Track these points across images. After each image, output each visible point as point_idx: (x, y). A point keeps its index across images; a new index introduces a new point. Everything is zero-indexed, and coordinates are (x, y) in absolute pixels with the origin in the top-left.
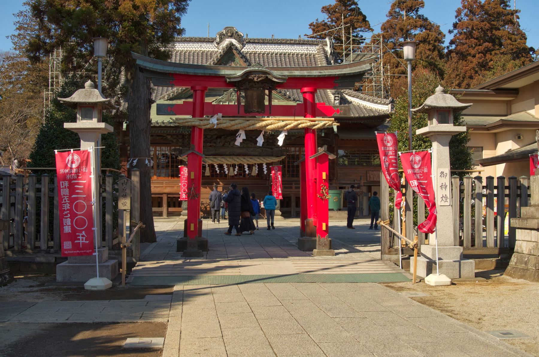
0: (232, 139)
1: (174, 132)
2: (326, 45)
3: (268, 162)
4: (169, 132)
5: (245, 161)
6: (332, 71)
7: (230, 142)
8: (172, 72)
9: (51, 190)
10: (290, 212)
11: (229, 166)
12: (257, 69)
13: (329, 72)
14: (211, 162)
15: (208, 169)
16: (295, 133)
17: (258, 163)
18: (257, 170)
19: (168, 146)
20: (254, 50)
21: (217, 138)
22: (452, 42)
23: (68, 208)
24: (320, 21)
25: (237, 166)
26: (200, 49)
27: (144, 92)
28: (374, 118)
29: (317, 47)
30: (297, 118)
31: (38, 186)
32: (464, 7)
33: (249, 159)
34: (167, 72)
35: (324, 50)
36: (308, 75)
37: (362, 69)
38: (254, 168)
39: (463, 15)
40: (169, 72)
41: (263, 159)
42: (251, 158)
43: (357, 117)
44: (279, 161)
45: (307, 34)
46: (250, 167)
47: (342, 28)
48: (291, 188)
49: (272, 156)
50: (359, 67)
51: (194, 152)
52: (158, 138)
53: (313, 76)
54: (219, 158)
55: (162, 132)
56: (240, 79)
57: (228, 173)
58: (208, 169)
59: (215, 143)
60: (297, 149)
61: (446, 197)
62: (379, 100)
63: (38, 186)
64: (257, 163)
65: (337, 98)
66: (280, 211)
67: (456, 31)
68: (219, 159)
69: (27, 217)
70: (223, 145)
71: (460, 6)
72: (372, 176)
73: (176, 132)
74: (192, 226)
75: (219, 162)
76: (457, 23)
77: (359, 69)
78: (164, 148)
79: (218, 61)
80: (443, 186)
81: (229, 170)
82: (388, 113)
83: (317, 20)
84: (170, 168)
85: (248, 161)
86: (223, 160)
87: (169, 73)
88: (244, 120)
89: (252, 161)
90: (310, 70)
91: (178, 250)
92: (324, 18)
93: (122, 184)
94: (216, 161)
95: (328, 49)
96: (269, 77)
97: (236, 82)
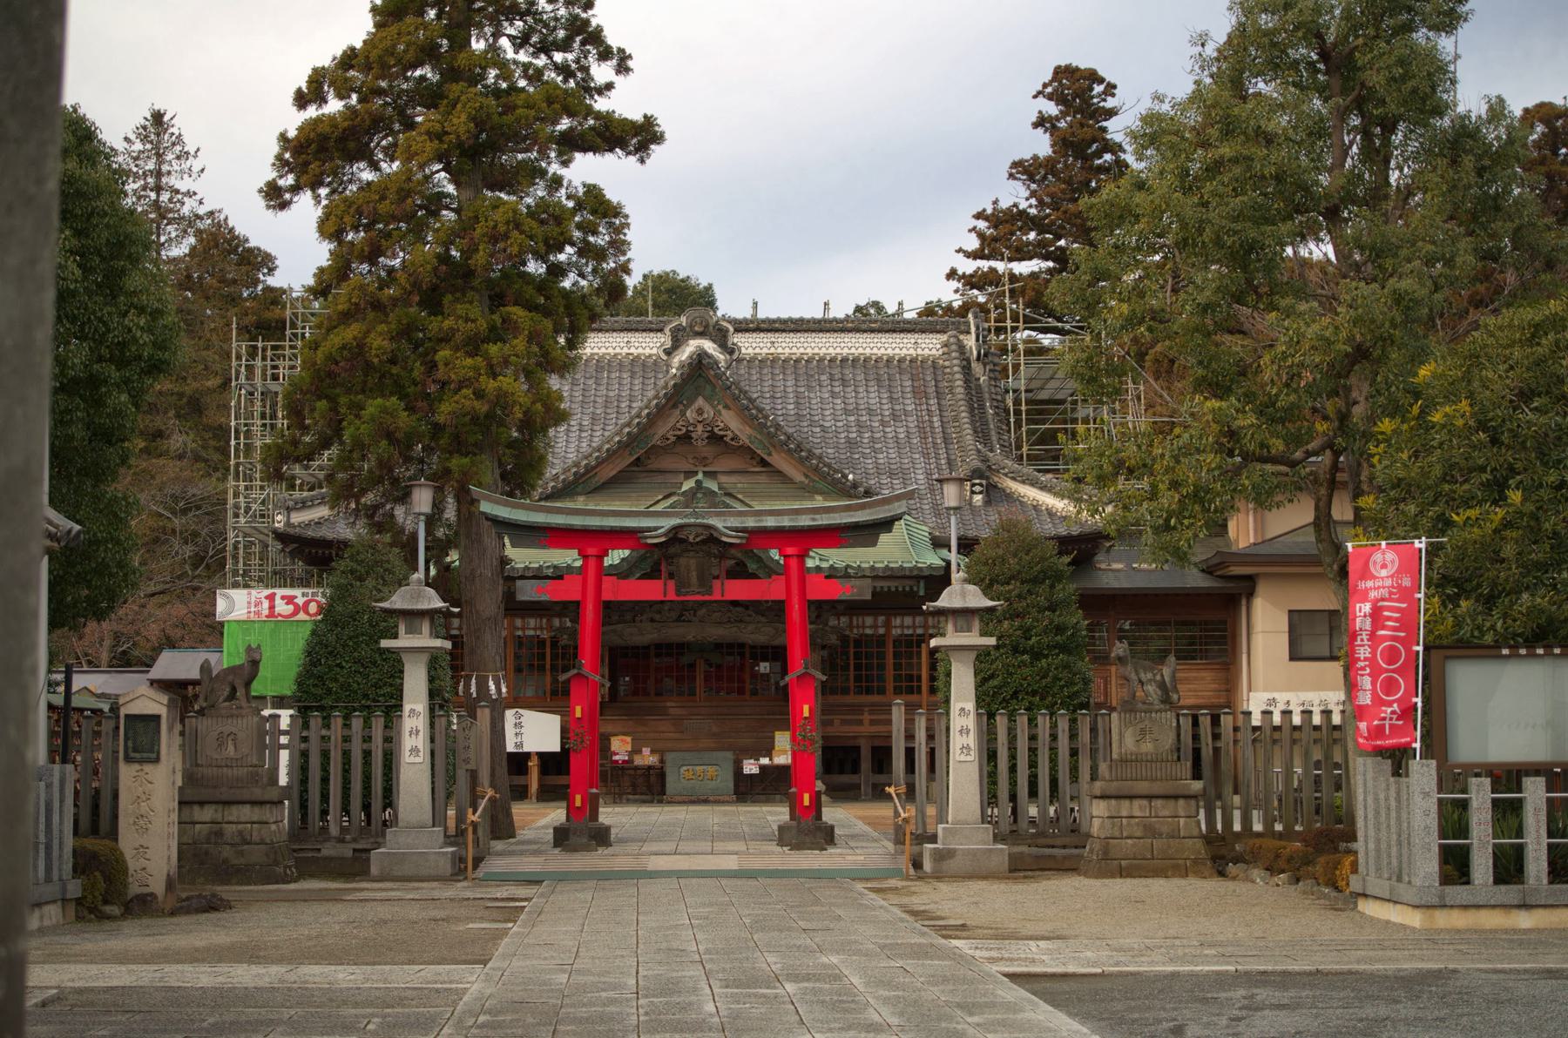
2: (968, 332)
9: (388, 740)
10: (858, 787)
19: (541, 617)
20: (772, 351)
23: (1368, 655)
24: (1005, 204)
26: (626, 350)
29: (944, 338)
31: (324, 732)
35: (961, 348)
45: (965, 248)
47: (1004, 292)
48: (860, 722)
56: (663, 539)
60: (881, 619)
61: (968, 748)
63: (324, 732)
65: (977, 489)
78: (532, 622)
79: (668, 400)
80: (964, 731)
83: (995, 202)
84: (548, 673)
91: (556, 846)
92: (1016, 195)
95: (970, 341)
96: (715, 534)
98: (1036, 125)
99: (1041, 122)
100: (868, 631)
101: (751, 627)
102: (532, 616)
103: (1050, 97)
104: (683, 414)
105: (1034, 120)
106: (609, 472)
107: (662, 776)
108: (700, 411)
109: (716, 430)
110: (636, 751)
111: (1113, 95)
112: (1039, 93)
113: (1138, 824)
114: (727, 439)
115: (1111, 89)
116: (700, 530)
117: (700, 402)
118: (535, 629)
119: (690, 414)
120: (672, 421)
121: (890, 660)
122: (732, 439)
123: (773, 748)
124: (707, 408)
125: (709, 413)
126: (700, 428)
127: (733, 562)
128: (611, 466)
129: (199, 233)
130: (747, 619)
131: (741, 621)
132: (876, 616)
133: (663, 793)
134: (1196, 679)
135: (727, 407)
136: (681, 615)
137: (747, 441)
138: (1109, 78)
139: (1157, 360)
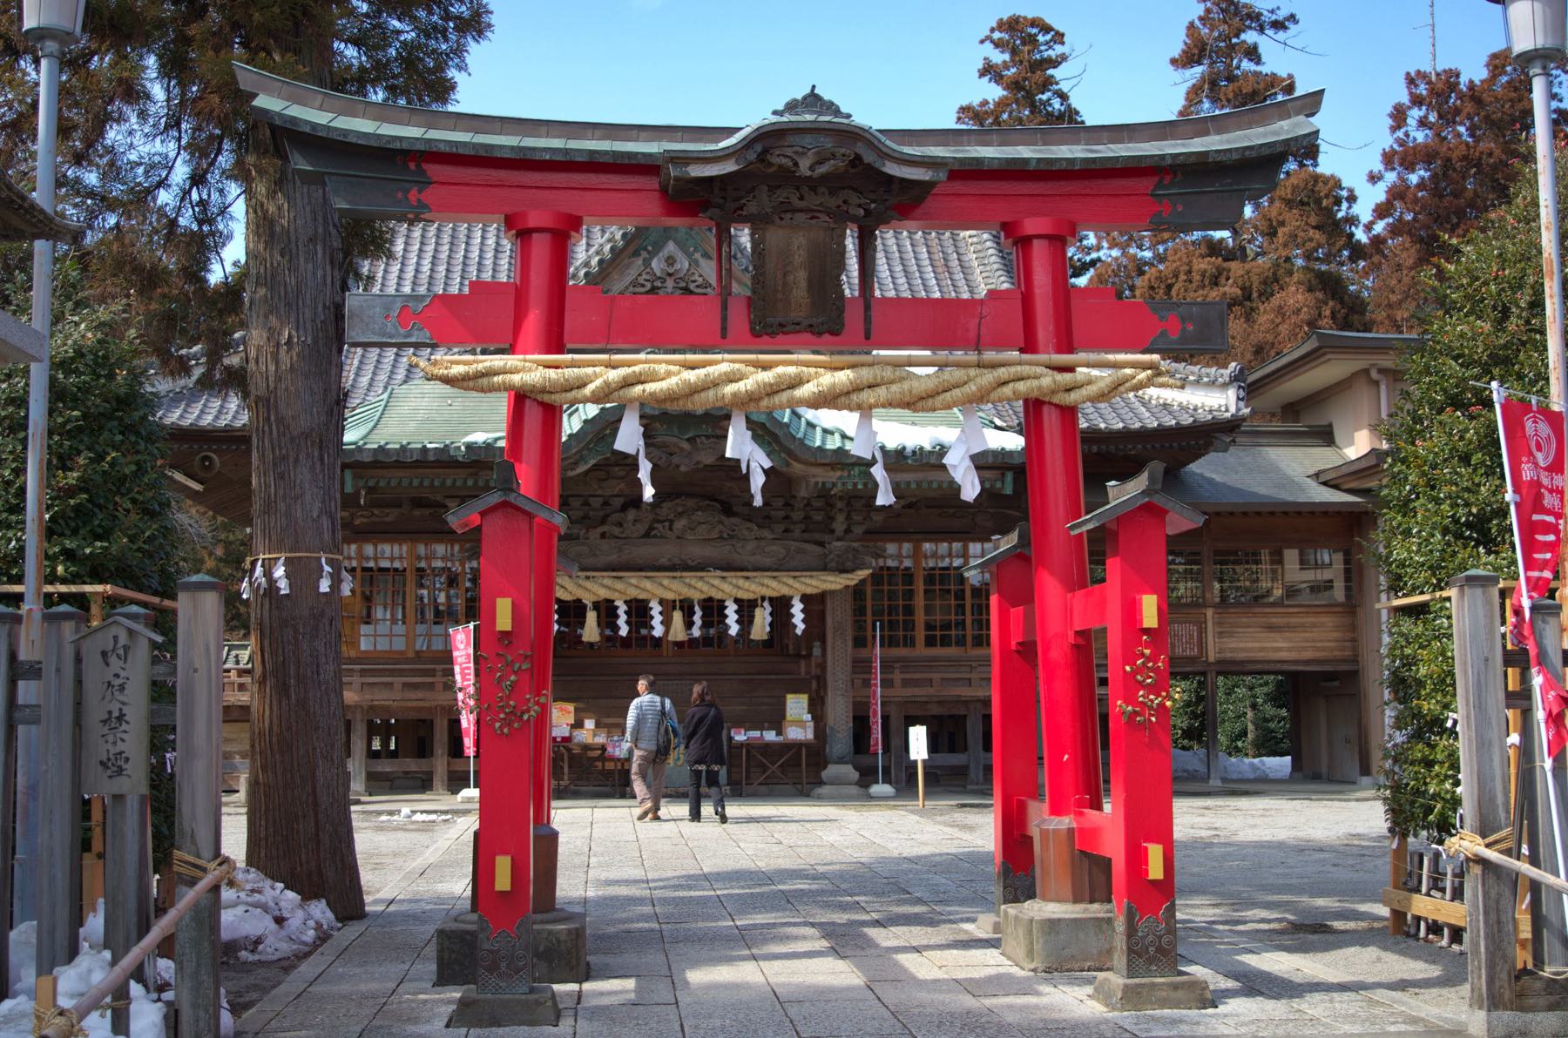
0: (680, 509)
1: (470, 483)
3: (809, 591)
4: (449, 482)
5: (726, 587)
6: (1142, 145)
7: (671, 522)
8: (419, 147)
11: (668, 607)
12: (809, 117)
13: (1128, 149)
14: (603, 594)
15: (591, 617)
16: (908, 483)
17: (774, 594)
18: (769, 619)
21: (624, 508)
22: (1381, 211)
25: (697, 608)
27: (314, 274)
28: (1179, 431)
30: (990, 355)
32: (1417, 101)
33: (741, 582)
34: (397, 145)
36: (1039, 160)
37: (1275, 133)
38: (758, 612)
39: (1412, 122)
40: (405, 146)
41: (791, 581)
42: (747, 578)
43: (1119, 432)
44: (847, 587)
46: (746, 610)
49: (825, 568)
50: (1261, 130)
51: (512, 498)
52: (417, 512)
53: (1064, 166)
54: (633, 578)
55: (426, 483)
56: (730, 167)
57: (667, 632)
58: (591, 617)
59: (620, 524)
62: (1193, 373)
64: (768, 593)
66: (856, 768)
67: (1391, 177)
68: (633, 581)
69: (1503, 629)
70: (647, 535)
71: (1404, 98)
73: (476, 482)
74: (503, 865)
75: (633, 593)
76: (1394, 152)
77: (1265, 135)
81: (667, 622)
82: (1228, 415)
85: (739, 588)
86: (647, 584)
87: (402, 151)
88: (747, 363)
89: (753, 587)
90: (1045, 144)
93: (104, 654)
94: (620, 589)
96: (869, 157)
97: (711, 179)
98: (983, 73)
99: (988, 70)
100: (890, 563)
101: (751, 546)
102: (440, 541)
103: (998, 44)
104: (647, 263)
105: (981, 67)
108: (670, 260)
109: (692, 286)
110: (578, 724)
111: (1063, 43)
112: (988, 38)
115: (1059, 37)
116: (828, 143)
117: (671, 247)
118: (443, 559)
119: (657, 265)
120: (632, 273)
121: (919, 601)
123: (783, 716)
124: (679, 255)
125: (683, 264)
126: (670, 283)
132: (900, 541)
134: (1314, 625)
136: (651, 528)
138: (1057, 26)
139: (1152, 288)
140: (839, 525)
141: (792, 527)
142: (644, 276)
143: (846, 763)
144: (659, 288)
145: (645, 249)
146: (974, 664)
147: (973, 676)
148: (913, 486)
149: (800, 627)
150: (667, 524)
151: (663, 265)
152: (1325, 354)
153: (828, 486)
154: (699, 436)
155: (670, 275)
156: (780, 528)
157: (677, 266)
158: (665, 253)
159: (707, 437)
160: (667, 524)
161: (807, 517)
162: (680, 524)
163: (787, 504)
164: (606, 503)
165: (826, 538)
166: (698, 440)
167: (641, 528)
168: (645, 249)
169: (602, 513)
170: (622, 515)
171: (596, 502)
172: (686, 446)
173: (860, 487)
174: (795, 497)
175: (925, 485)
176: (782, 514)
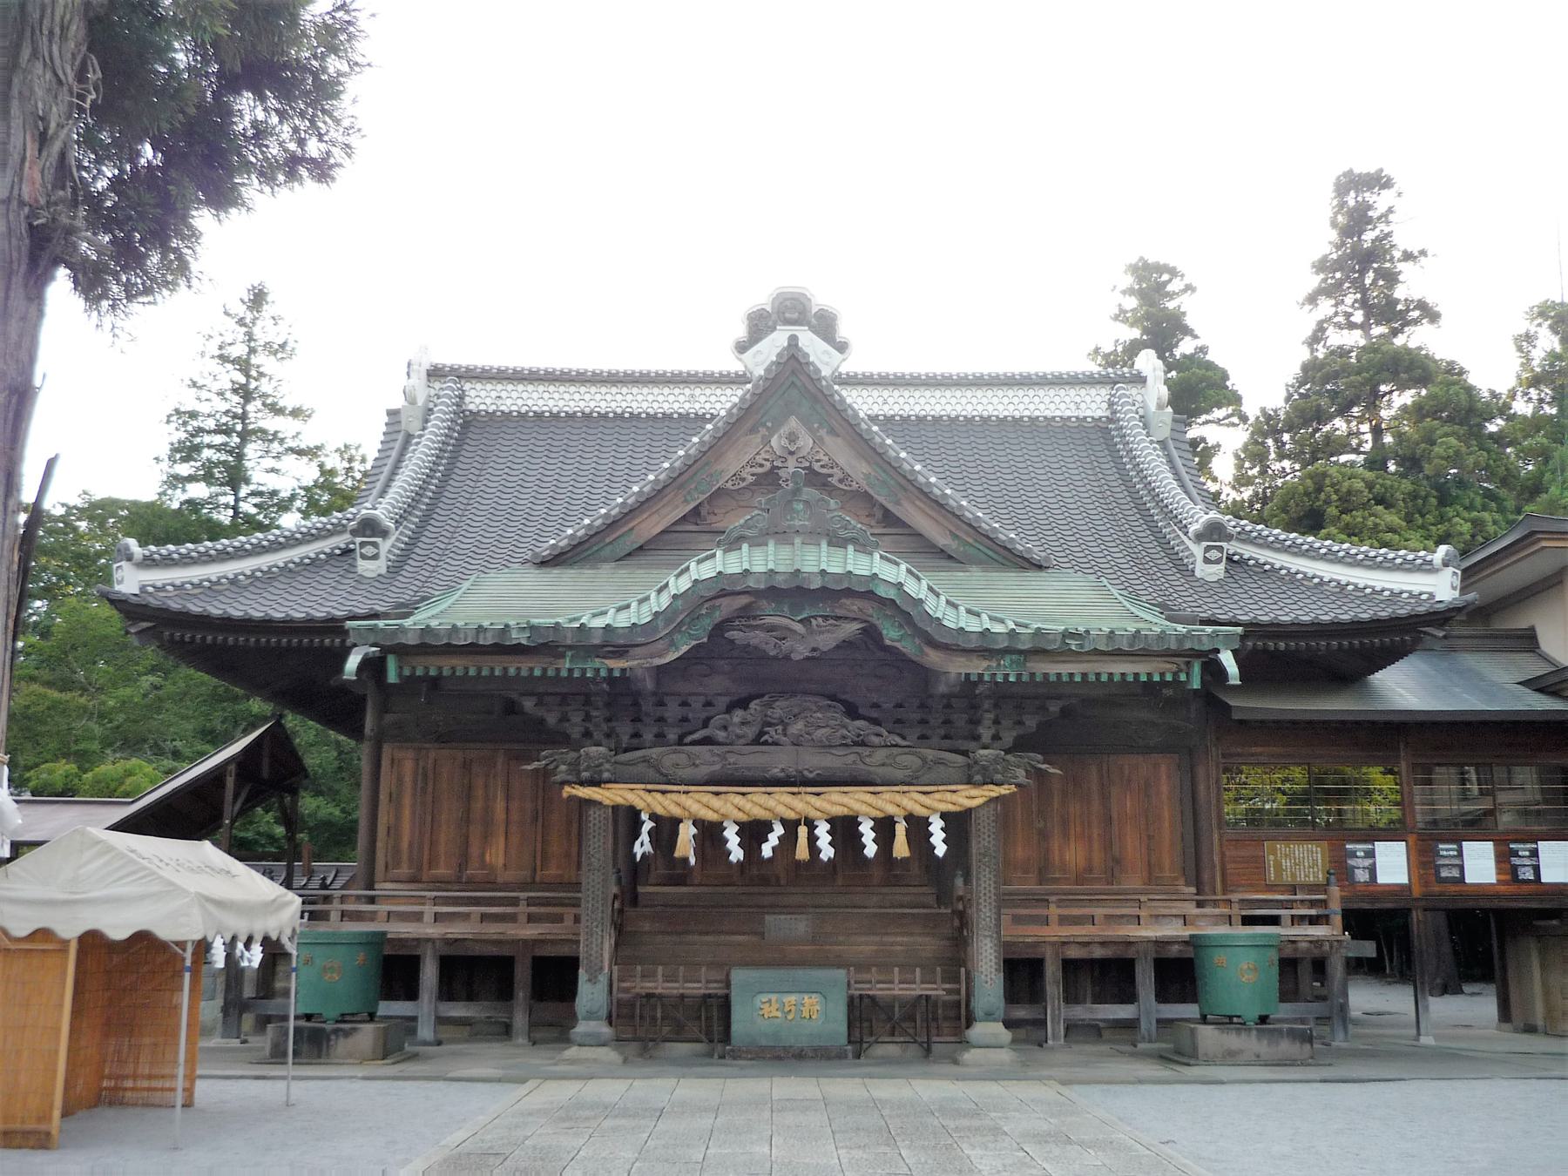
48: (1046, 921)
59: (725, 728)
72: (1286, 863)
106: (651, 525)
107: (725, 1004)
109: (816, 467)
113: (145, 788)
114: (834, 481)
117: (793, 423)
122: (841, 481)
125: (806, 442)
127: (856, 626)
128: (655, 518)
129: (95, 234)
130: (876, 740)
131: (863, 744)
133: (726, 1036)
135: (833, 432)
136: (762, 733)
137: (864, 484)
140: (986, 734)
141: (929, 733)
142: (764, 455)
143: (995, 1020)
144: (779, 468)
145: (764, 425)
146: (1143, 898)
147: (1143, 913)
148: (1078, 679)
149: (941, 850)
150: (780, 728)
151: (784, 442)
152: (1540, 540)
153: (974, 678)
154: (815, 617)
155: (792, 453)
156: (913, 734)
157: (800, 443)
158: (784, 430)
159: (825, 618)
160: (780, 728)
161: (947, 722)
162: (797, 727)
163: (922, 706)
164: (708, 704)
165: (972, 745)
166: (814, 622)
167: (751, 732)
168: (764, 425)
169: (704, 715)
170: (727, 716)
171: (696, 703)
172: (799, 628)
173: (1012, 679)
174: (931, 696)
175: (1092, 678)
176: (917, 716)
